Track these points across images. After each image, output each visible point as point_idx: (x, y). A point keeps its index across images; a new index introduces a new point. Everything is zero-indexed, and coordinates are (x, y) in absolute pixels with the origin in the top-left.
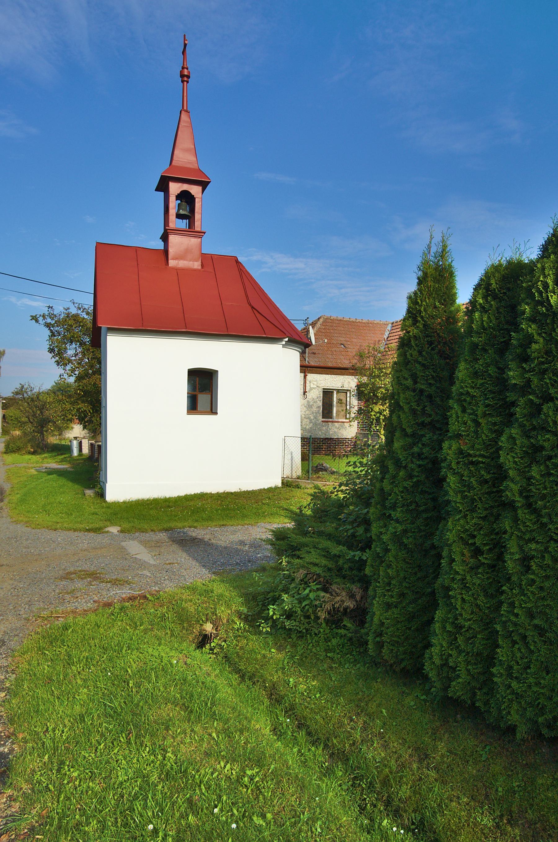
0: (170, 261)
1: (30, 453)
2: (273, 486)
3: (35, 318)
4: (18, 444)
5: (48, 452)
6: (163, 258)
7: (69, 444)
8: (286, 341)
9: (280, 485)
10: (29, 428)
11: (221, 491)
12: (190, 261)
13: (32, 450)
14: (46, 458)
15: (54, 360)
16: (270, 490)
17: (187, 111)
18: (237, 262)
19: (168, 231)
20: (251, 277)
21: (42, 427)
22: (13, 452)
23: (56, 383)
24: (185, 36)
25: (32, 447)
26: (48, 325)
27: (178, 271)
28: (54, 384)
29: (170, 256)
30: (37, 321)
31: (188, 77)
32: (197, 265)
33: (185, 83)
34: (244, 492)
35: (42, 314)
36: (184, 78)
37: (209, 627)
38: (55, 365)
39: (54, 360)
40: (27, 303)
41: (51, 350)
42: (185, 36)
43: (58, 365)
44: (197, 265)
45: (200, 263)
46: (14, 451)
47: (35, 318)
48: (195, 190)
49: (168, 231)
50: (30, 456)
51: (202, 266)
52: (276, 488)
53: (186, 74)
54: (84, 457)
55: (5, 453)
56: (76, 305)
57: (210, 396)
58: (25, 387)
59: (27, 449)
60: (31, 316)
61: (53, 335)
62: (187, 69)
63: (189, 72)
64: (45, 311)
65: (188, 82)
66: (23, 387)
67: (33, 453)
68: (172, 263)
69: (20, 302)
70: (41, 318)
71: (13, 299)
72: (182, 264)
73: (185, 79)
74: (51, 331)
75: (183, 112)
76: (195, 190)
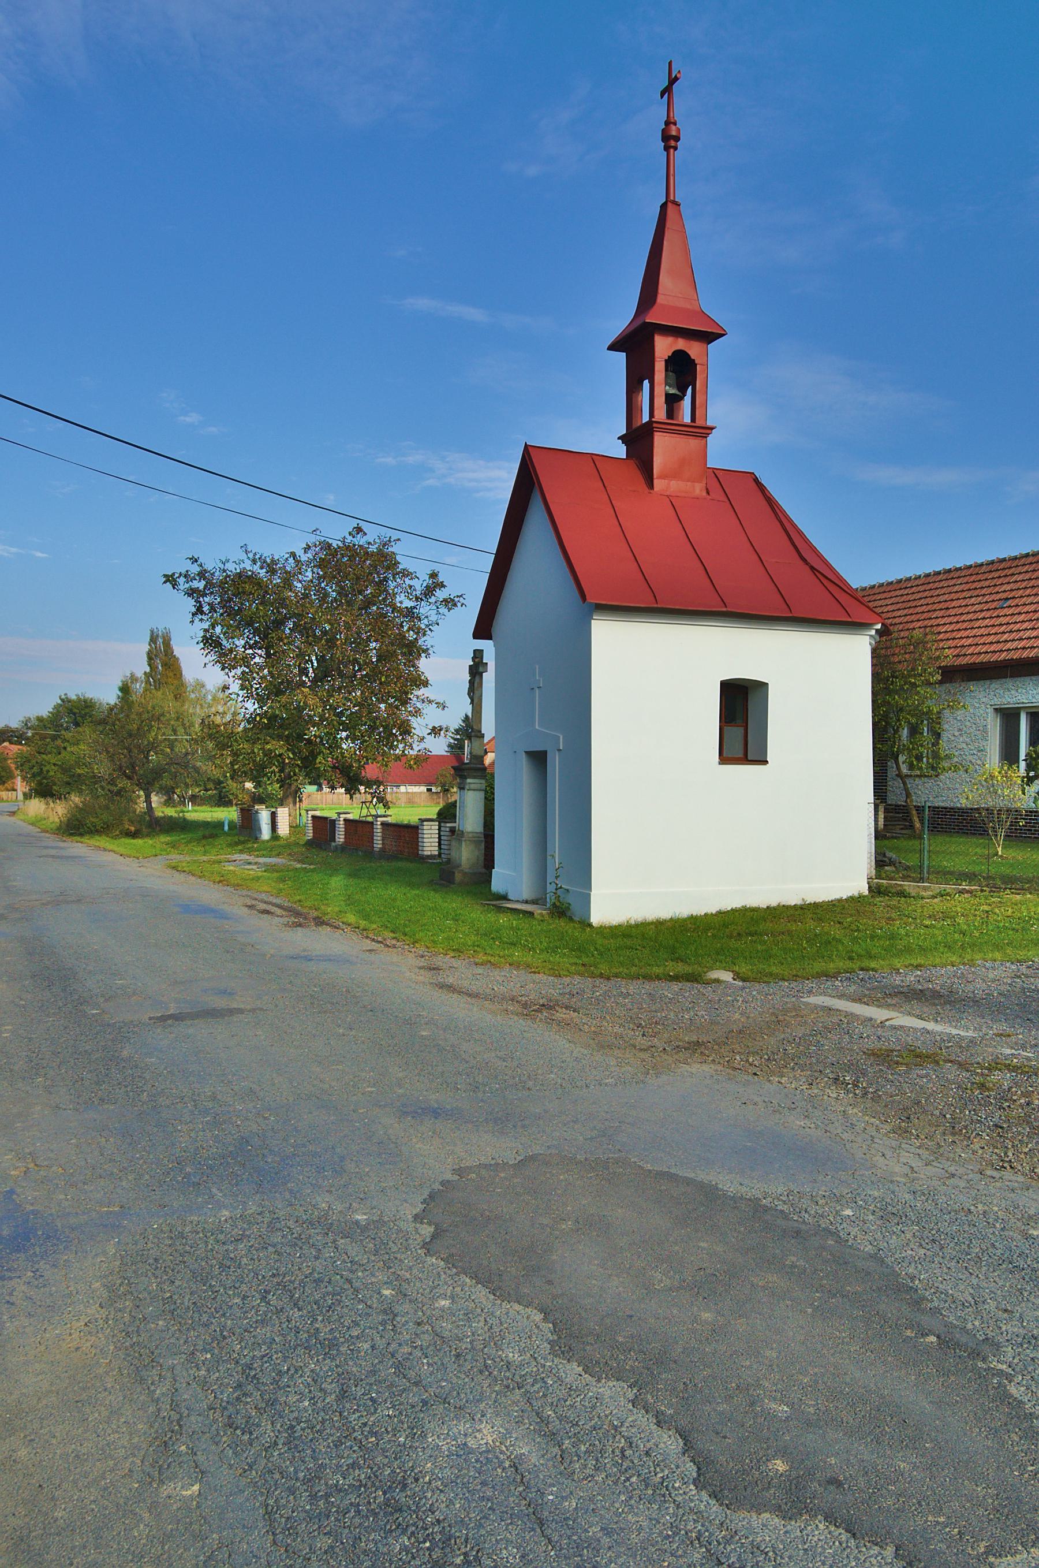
0: (656, 482)
2: (856, 894)
3: (170, 579)
8: (877, 630)
9: (866, 893)
11: (774, 903)
12: (688, 481)
13: (133, 829)
16: (851, 899)
18: (756, 481)
19: (655, 425)
20: (783, 512)
23: (62, 700)
24: (670, 63)
26: (191, 592)
28: (59, 702)
31: (677, 139)
33: (672, 150)
34: (810, 904)
35: (184, 572)
36: (669, 140)
42: (670, 63)
44: (698, 489)
46: (97, 831)
47: (170, 579)
48: (694, 349)
49: (655, 425)
52: (861, 896)
53: (674, 133)
54: (282, 842)
56: (251, 555)
57: (741, 730)
59: (121, 828)
60: (165, 576)
62: (675, 124)
63: (678, 130)
65: (676, 148)
72: (675, 486)
73: (673, 143)
75: (669, 204)
76: (694, 349)
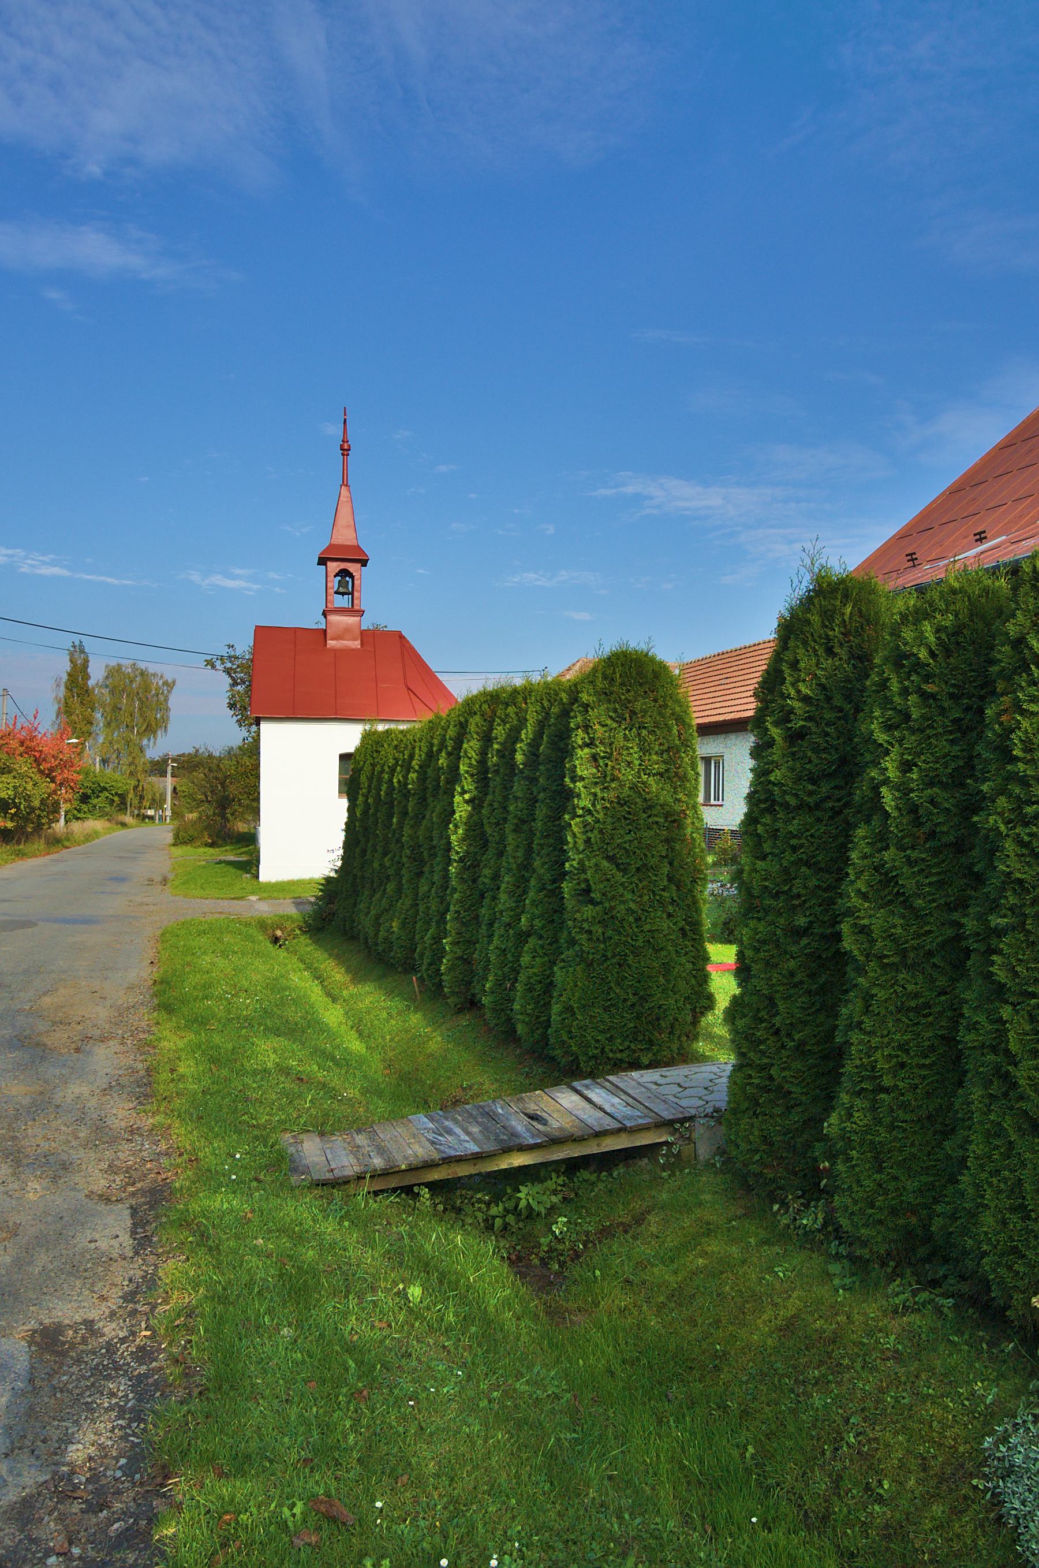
0: (329, 642)
1: (207, 845)
3: (211, 664)
4: (191, 832)
5: (232, 843)
6: (322, 636)
7: (252, 831)
10: (209, 810)
14: (226, 851)
15: (235, 718)
17: (347, 485)
21: (224, 808)
22: (185, 843)
25: (210, 836)
26: (228, 671)
27: (335, 651)
29: (328, 637)
30: (213, 667)
32: (357, 644)
36: (345, 451)
37: (279, 933)
38: (236, 726)
39: (235, 718)
40: (218, 583)
41: (232, 706)
43: (241, 726)
44: (357, 644)
45: (359, 642)
48: (352, 567)
50: (207, 849)
51: (362, 644)
55: (174, 845)
58: (201, 751)
61: (235, 683)
64: (224, 652)
66: (197, 751)
67: (212, 845)
68: (331, 643)
69: (207, 582)
70: (219, 662)
71: (195, 577)
74: (233, 679)
76: (352, 567)
